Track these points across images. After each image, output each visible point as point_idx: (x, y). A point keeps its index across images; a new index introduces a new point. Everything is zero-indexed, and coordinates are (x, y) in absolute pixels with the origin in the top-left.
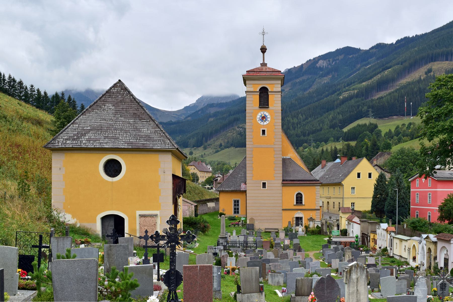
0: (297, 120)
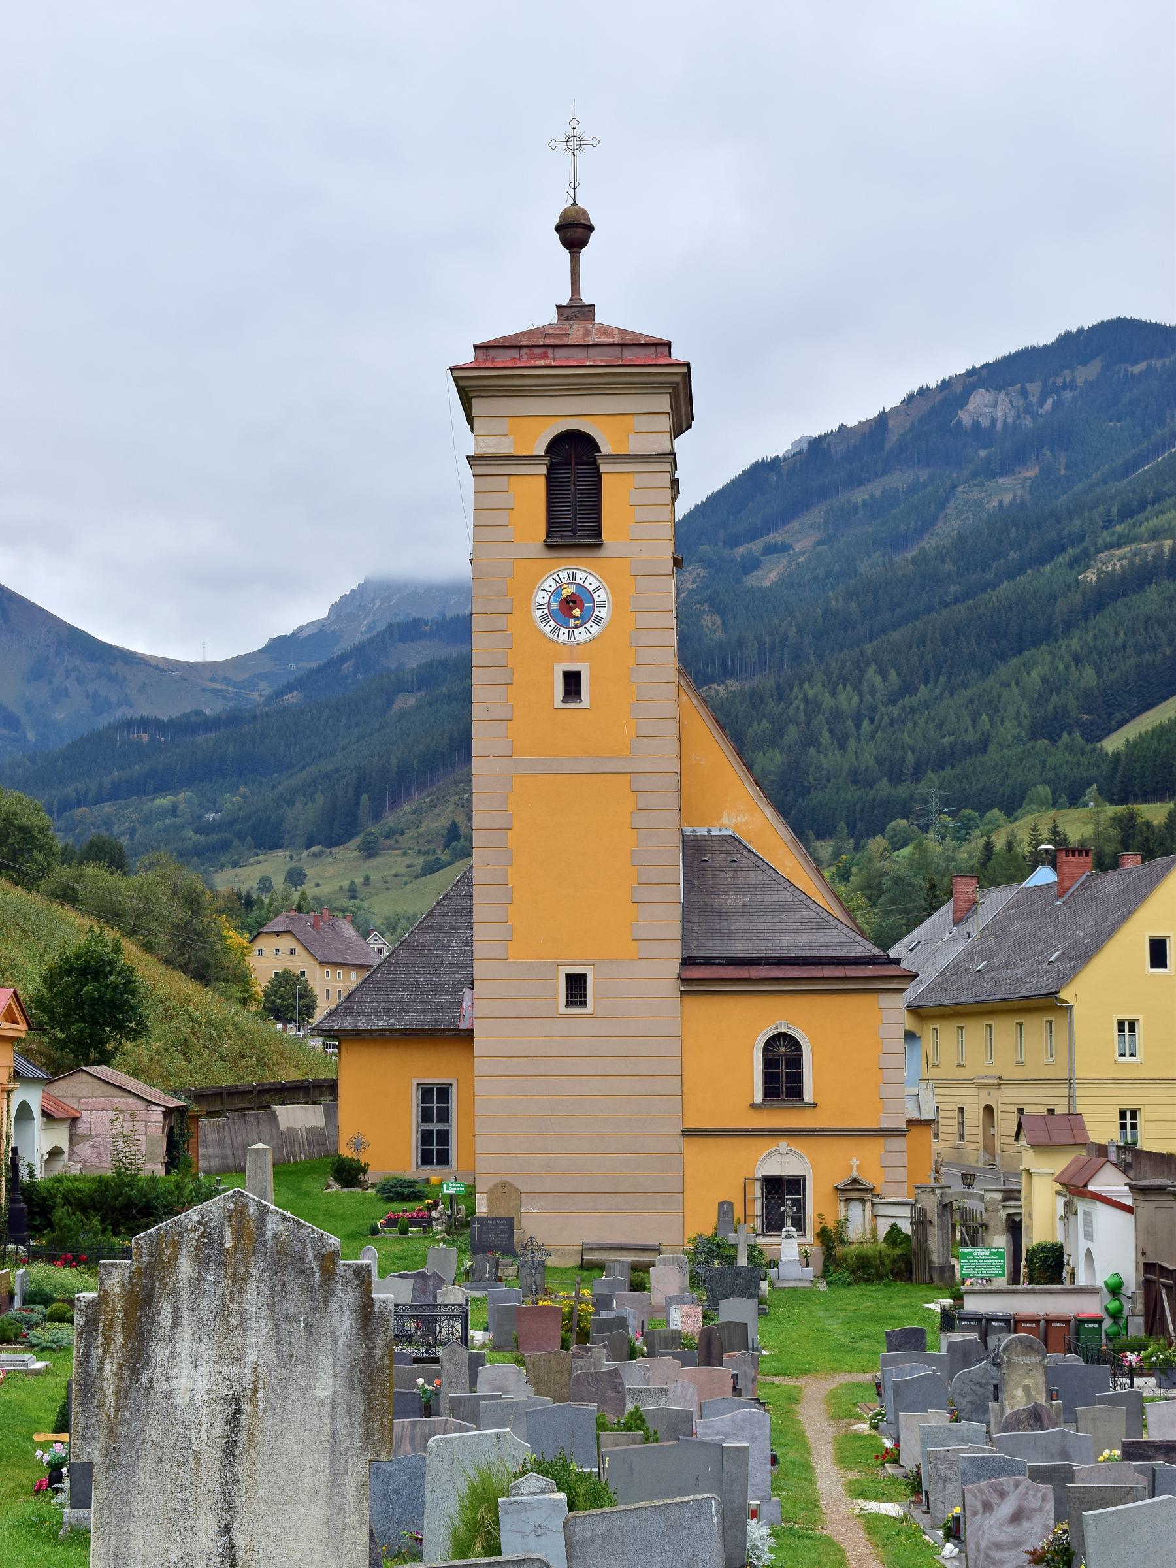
0: (856, 699)
